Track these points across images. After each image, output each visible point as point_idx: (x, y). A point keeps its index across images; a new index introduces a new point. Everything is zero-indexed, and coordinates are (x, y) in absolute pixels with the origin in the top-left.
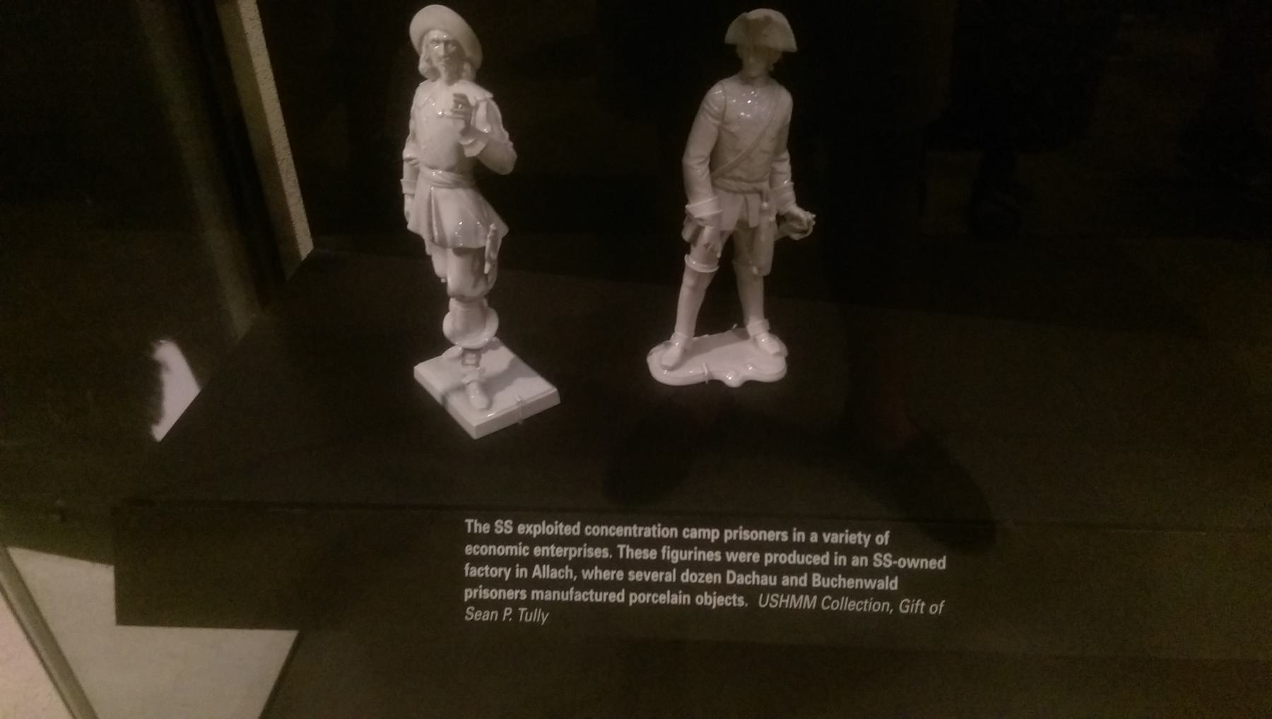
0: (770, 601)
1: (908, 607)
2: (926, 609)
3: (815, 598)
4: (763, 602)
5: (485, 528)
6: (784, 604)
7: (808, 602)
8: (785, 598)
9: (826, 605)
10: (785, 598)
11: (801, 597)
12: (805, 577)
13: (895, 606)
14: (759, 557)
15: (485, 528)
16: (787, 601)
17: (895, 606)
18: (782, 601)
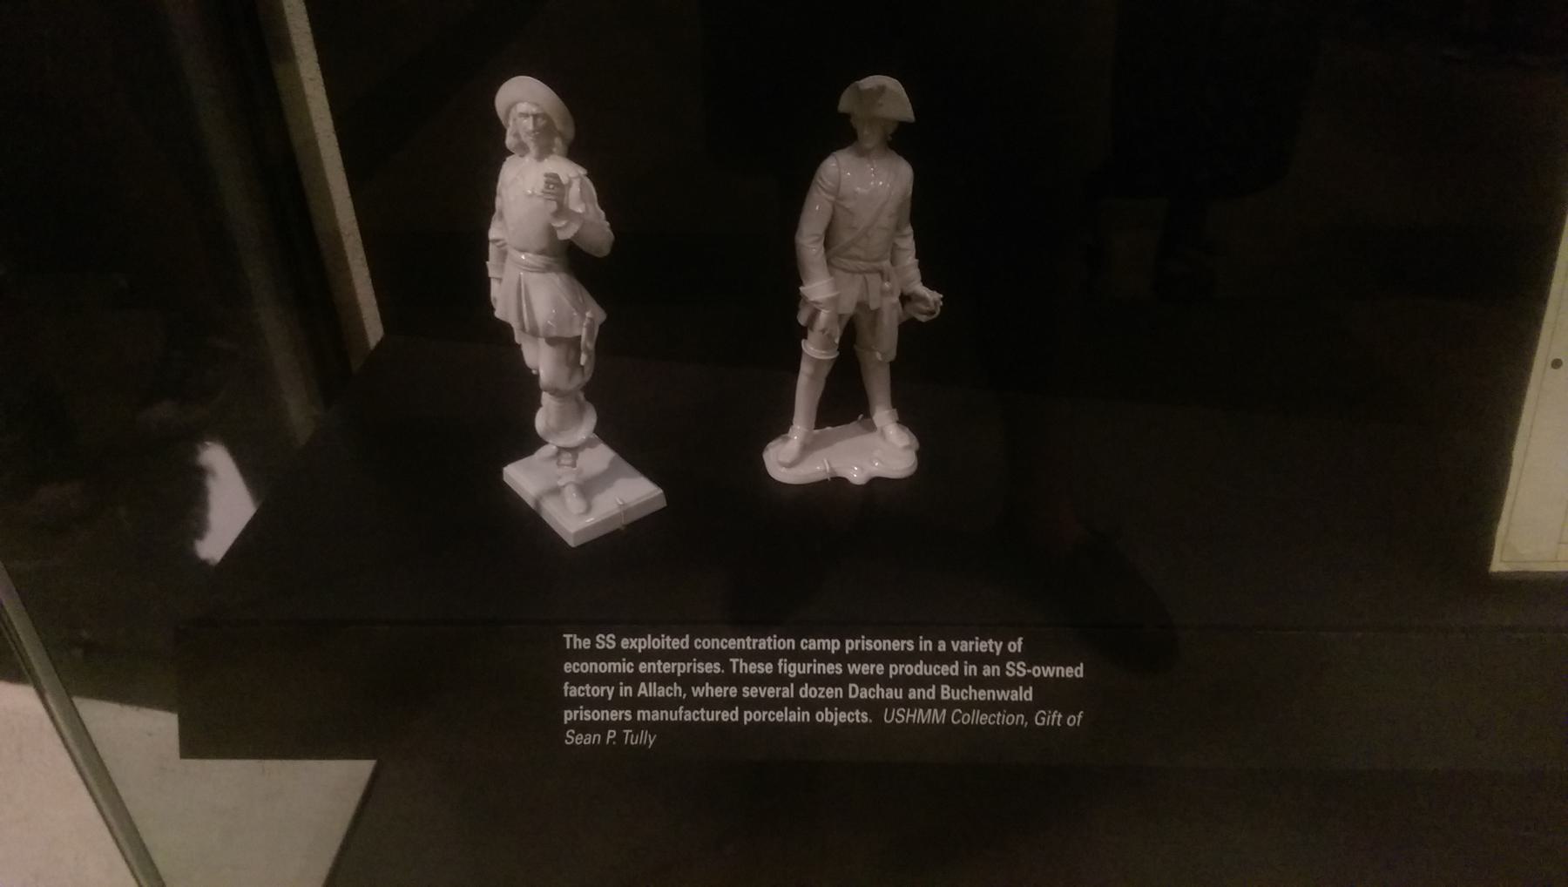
0: (896, 716)
1: (1043, 719)
2: (1064, 720)
3: (944, 711)
4: (889, 718)
5: (586, 643)
6: (911, 719)
7: (936, 716)
8: (912, 712)
9: (955, 720)
10: (912, 712)
11: (930, 711)
12: (956, 666)
13: (1030, 718)
14: (589, 642)
15: (586, 643)
16: (914, 716)
17: (1030, 718)
18: (908, 715)
